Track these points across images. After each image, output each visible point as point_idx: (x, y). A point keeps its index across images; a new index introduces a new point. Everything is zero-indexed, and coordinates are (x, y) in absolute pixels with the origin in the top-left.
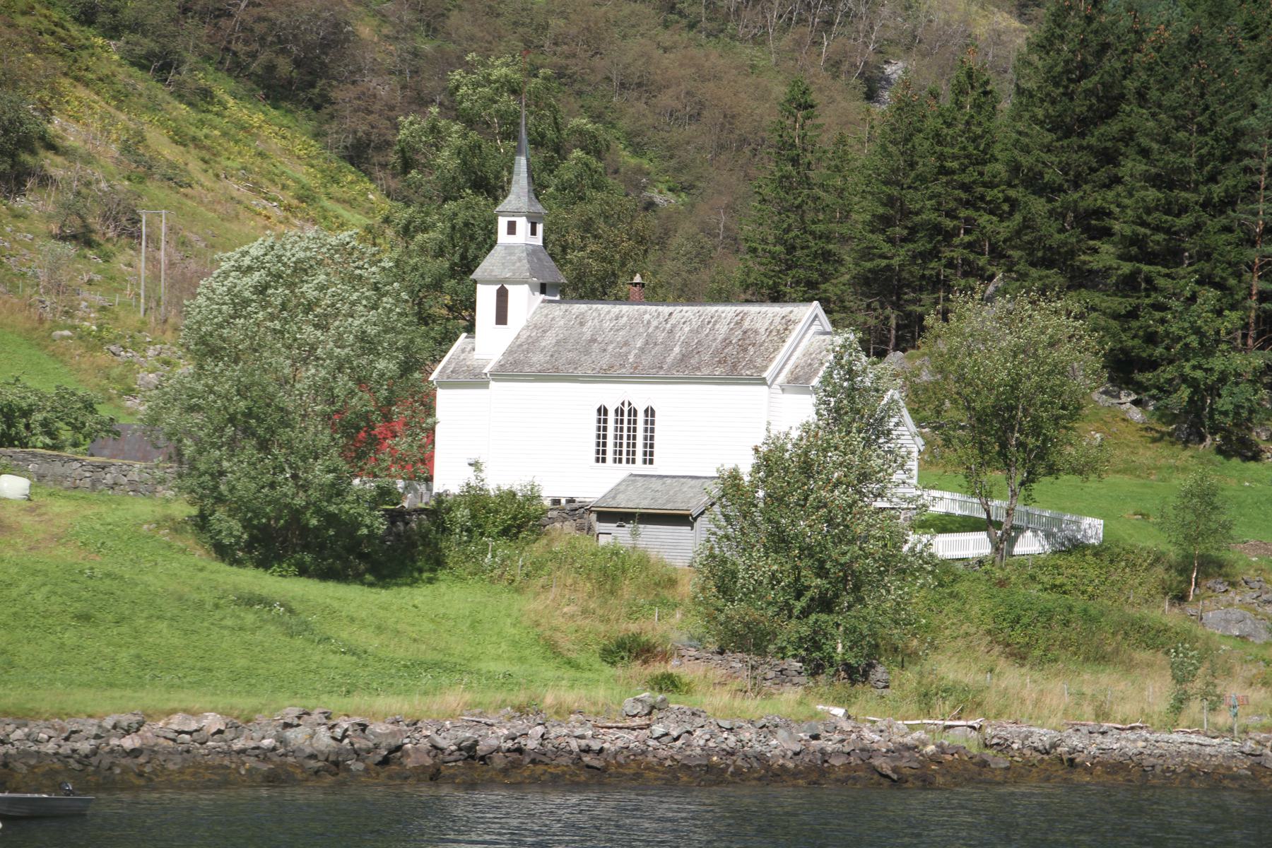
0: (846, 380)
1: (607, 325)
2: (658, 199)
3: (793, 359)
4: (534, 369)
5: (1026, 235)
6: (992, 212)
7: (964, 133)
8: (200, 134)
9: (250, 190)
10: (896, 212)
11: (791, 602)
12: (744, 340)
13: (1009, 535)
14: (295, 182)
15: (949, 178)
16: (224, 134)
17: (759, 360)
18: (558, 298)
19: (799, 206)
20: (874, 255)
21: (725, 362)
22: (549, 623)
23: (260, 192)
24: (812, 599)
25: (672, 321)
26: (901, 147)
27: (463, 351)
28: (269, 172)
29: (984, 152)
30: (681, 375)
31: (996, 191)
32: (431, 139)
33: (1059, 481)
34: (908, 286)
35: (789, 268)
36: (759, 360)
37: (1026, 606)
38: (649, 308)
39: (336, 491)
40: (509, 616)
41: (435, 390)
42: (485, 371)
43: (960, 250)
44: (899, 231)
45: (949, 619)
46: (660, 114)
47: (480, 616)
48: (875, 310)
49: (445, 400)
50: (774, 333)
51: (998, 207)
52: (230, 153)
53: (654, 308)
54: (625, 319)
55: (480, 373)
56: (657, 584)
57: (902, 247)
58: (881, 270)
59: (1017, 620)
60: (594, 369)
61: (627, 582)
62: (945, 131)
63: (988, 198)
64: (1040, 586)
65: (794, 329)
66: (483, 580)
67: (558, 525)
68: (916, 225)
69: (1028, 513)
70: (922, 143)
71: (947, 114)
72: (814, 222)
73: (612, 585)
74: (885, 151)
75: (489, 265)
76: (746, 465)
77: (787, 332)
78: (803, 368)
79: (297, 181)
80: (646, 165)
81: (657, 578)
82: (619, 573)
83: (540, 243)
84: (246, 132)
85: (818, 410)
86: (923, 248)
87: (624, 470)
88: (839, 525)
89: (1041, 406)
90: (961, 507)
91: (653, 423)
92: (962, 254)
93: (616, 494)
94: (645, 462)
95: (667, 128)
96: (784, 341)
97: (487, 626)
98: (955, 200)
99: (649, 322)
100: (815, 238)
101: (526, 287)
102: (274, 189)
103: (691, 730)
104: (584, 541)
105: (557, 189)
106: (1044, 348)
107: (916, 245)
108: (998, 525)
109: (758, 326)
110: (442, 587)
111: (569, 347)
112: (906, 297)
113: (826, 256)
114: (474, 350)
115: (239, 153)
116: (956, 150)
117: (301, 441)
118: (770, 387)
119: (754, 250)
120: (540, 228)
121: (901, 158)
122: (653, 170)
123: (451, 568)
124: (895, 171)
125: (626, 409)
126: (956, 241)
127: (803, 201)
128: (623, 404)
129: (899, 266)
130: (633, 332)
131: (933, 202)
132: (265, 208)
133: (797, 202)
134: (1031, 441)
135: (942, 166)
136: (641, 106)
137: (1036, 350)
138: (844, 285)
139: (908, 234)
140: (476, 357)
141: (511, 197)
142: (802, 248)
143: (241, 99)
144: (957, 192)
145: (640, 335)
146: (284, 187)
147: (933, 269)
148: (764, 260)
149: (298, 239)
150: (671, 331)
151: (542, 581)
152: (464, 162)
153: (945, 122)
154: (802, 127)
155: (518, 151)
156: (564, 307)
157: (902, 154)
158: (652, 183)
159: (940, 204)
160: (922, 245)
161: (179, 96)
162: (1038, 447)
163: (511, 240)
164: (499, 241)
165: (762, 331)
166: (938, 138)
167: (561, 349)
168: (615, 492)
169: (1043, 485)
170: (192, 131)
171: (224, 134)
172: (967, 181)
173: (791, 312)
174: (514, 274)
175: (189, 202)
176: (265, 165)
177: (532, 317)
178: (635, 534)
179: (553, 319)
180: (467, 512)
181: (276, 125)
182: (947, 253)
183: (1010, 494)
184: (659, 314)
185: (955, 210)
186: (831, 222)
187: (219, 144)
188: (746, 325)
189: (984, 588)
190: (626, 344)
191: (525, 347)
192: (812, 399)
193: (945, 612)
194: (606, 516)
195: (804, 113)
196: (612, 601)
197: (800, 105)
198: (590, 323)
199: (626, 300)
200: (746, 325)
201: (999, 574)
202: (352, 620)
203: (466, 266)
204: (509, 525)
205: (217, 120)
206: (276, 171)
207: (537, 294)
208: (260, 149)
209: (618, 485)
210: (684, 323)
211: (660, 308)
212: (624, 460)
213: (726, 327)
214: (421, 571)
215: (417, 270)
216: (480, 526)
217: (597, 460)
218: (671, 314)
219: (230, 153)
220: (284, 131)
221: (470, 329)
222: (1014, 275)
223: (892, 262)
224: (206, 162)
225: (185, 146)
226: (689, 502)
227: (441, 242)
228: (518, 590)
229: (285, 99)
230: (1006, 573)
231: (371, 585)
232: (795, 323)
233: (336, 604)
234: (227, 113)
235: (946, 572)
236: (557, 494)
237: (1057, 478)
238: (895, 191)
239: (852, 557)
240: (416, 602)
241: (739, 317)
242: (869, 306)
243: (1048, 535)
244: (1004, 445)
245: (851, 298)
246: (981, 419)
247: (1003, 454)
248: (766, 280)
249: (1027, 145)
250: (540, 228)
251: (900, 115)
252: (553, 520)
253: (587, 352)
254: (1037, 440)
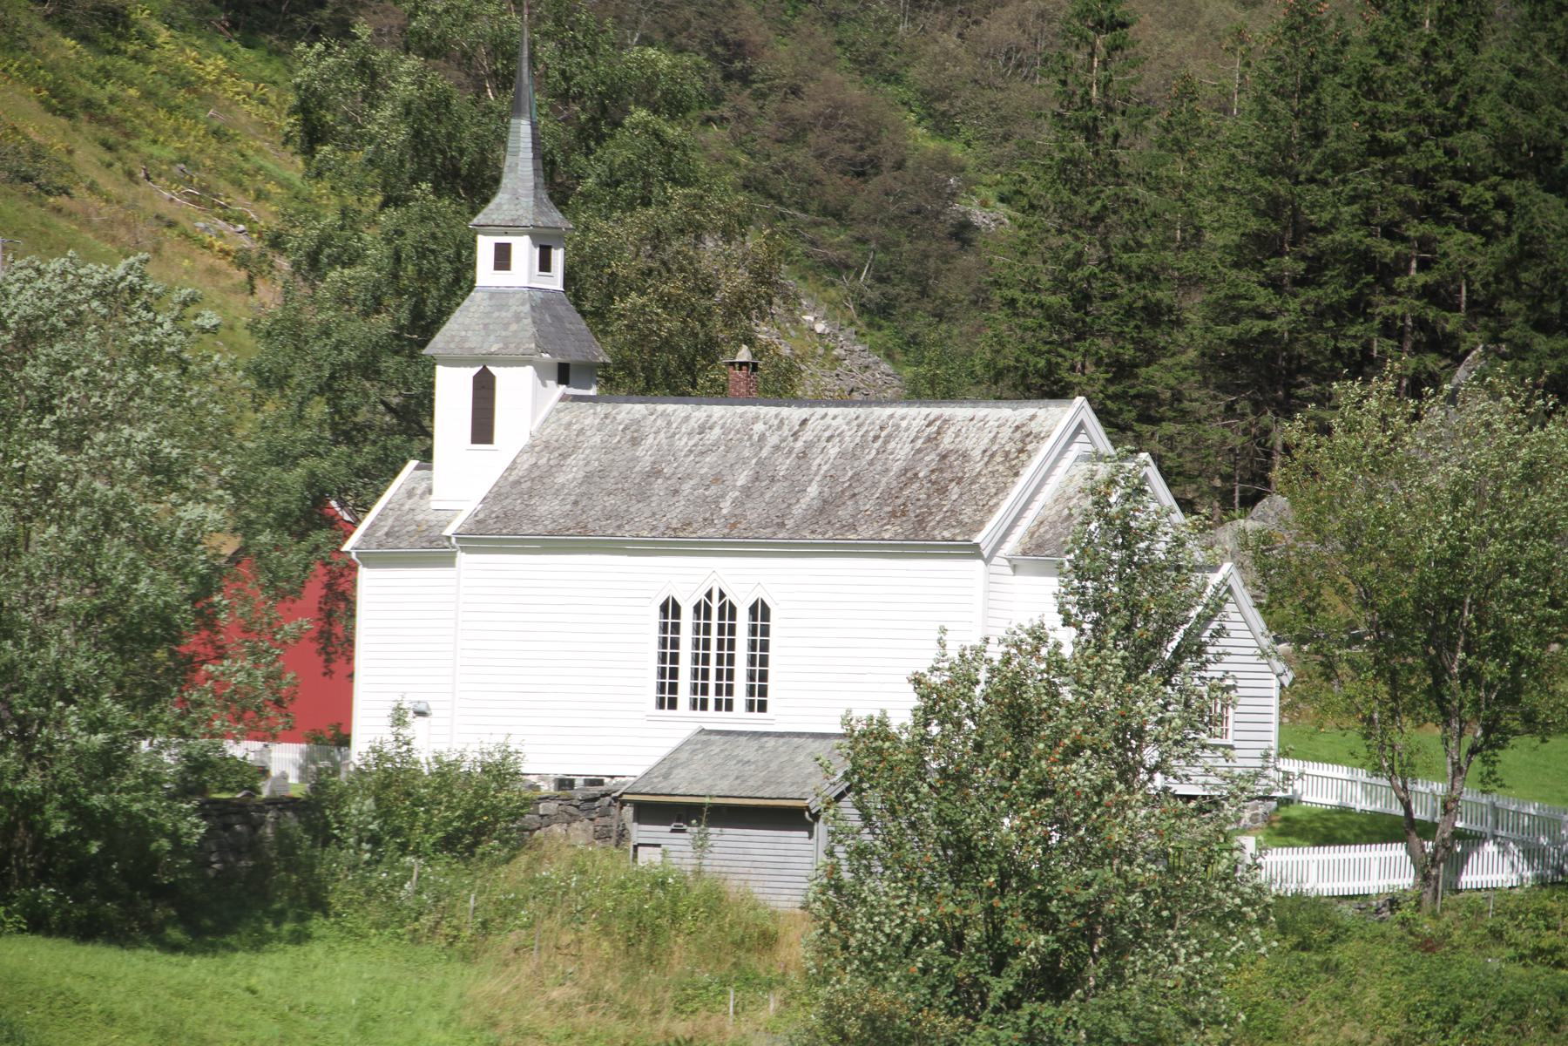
0: (1116, 547)
1: (682, 443)
2: (978, 216)
3: (1035, 508)
4: (540, 528)
5: (1526, 270)
6: (1474, 228)
7: (1418, 74)
8: (101, 95)
9: (195, 201)
10: (1285, 229)
11: (983, 978)
12: (941, 471)
13: (1449, 849)
14: (281, 186)
15: (1389, 161)
16: (148, 95)
17: (968, 511)
18: (593, 391)
19: (1098, 219)
20: (1240, 311)
21: (904, 513)
22: (515, 1020)
23: (214, 205)
24: (1026, 973)
25: (807, 436)
26: (1295, 102)
27: (410, 494)
28: (232, 168)
29: (1458, 110)
30: (818, 539)
31: (1479, 188)
32: (360, 86)
33: (1545, 747)
34: (1307, 370)
35: (1080, 337)
36: (968, 511)
37: (1474, 989)
38: (763, 410)
39: (110, 763)
40: (438, 1007)
41: (352, 568)
42: (448, 532)
43: (1410, 301)
44: (1289, 265)
45: (1317, 1013)
46: (987, 55)
47: (379, 1008)
48: (1243, 416)
49: (371, 585)
50: (999, 459)
51: (1486, 218)
52: (159, 132)
53: (773, 410)
54: (717, 431)
55: (440, 538)
56: (739, 944)
57: (1295, 296)
58: (1254, 340)
59: (1454, 1017)
60: (654, 528)
61: (680, 940)
62: (1382, 71)
63: (1465, 201)
64: (1511, 952)
65: (1036, 450)
66: (399, 937)
67: (557, 829)
68: (1323, 253)
69: (1495, 810)
70: (1335, 95)
71: (1387, 37)
72: (1126, 248)
73: (653, 945)
74: (1265, 110)
75: (461, 327)
76: (901, 710)
77: (1023, 457)
78: (1053, 525)
79: (285, 184)
80: (956, 150)
81: (739, 931)
82: (664, 922)
83: (559, 286)
84: (189, 91)
85: (1062, 605)
86: (1335, 298)
87: (713, 719)
88: (1077, 827)
89: (1509, 600)
90: (1368, 794)
91: (766, 631)
92: (1412, 309)
93: (671, 768)
94: (750, 707)
95: (999, 82)
96: (1017, 474)
97: (391, 1027)
98: (1400, 203)
99: (762, 438)
100: (1129, 279)
101: (529, 370)
102: (240, 198)
104: (602, 858)
105: (602, 184)
106: (1516, 486)
107: (1321, 292)
108: (1427, 830)
109: (969, 444)
110: (317, 951)
111: (609, 484)
112: (1300, 392)
113: (1154, 314)
114: (430, 491)
115: (176, 131)
116: (1401, 108)
117: (31, 667)
118: (987, 561)
119: (1012, 302)
120: (558, 257)
121: (1296, 124)
122: (972, 162)
123: (338, 915)
124: (1284, 149)
125: (715, 606)
126: (1401, 283)
127: (1104, 207)
128: (709, 595)
129: (1290, 332)
130: (732, 456)
131: (1355, 208)
132: (221, 236)
133: (1093, 210)
134: (1490, 667)
135: (1374, 138)
136: (950, 41)
137: (1498, 490)
138: (1184, 369)
139: (1307, 270)
140: (434, 505)
141: (501, 198)
142: (1104, 299)
143: (182, 29)
144: (1402, 188)
145: (745, 461)
146: (260, 196)
147: (1355, 337)
148: (1029, 322)
149: (34, 274)
150: (804, 455)
151: (512, 939)
152: (417, 134)
153: (1381, 54)
154: (1105, 65)
155: (516, 110)
156: (602, 409)
157: (1297, 116)
158: (969, 186)
159: (1370, 212)
160: (1333, 290)
161: (62, 22)
162: (1501, 679)
163: (502, 279)
164: (478, 284)
165: (977, 454)
166: (1368, 85)
167: (593, 490)
168: (669, 764)
169: (1517, 755)
170: (86, 89)
171: (148, 95)
172: (1421, 166)
173: (1033, 417)
174: (506, 346)
175: (63, 223)
176: (224, 155)
177: (541, 429)
178: (701, 846)
179: (581, 432)
180: (370, 803)
181: (248, 78)
182: (1383, 307)
183: (1450, 769)
184: (782, 422)
185: (1397, 224)
186: (1165, 248)
187: (138, 115)
188: (946, 442)
189: (1394, 952)
190: (717, 479)
191: (525, 486)
192: (1052, 584)
193: (1309, 1000)
194: (654, 811)
195: (1108, 37)
196: (649, 976)
197: (1100, 23)
198: (650, 440)
199: (720, 393)
200: (946, 442)
201: (1427, 927)
202: (110, 1018)
203: (425, 324)
204: (458, 830)
205: (136, 69)
206: (246, 166)
207: (552, 383)
208: (216, 123)
209: (677, 750)
210: (829, 439)
211: (785, 411)
212: (711, 704)
213: (908, 448)
214: (279, 918)
215: (328, 336)
216: (397, 832)
217: (661, 704)
218: (804, 422)
219: (159, 132)
220: (264, 89)
221: (427, 456)
222: (1504, 347)
223: (1274, 325)
224: (109, 148)
225: (71, 117)
226: (805, 784)
227: (377, 285)
228: (467, 958)
229: (269, 28)
230: (1442, 925)
231: (175, 948)
232: (1039, 438)
233: (82, 988)
234: (154, 55)
235: (1320, 922)
236: (562, 771)
237: (1544, 741)
238: (1282, 188)
239: (1101, 892)
240: (253, 981)
241: (934, 429)
242: (1230, 407)
243: (1531, 853)
244: (1437, 670)
245: (1195, 395)
246: (1390, 627)
247: (1436, 694)
248: (1032, 359)
249: (1530, 95)
250: (558, 257)
251: (1292, 39)
252: (547, 820)
253: (643, 496)
254: (1501, 667)
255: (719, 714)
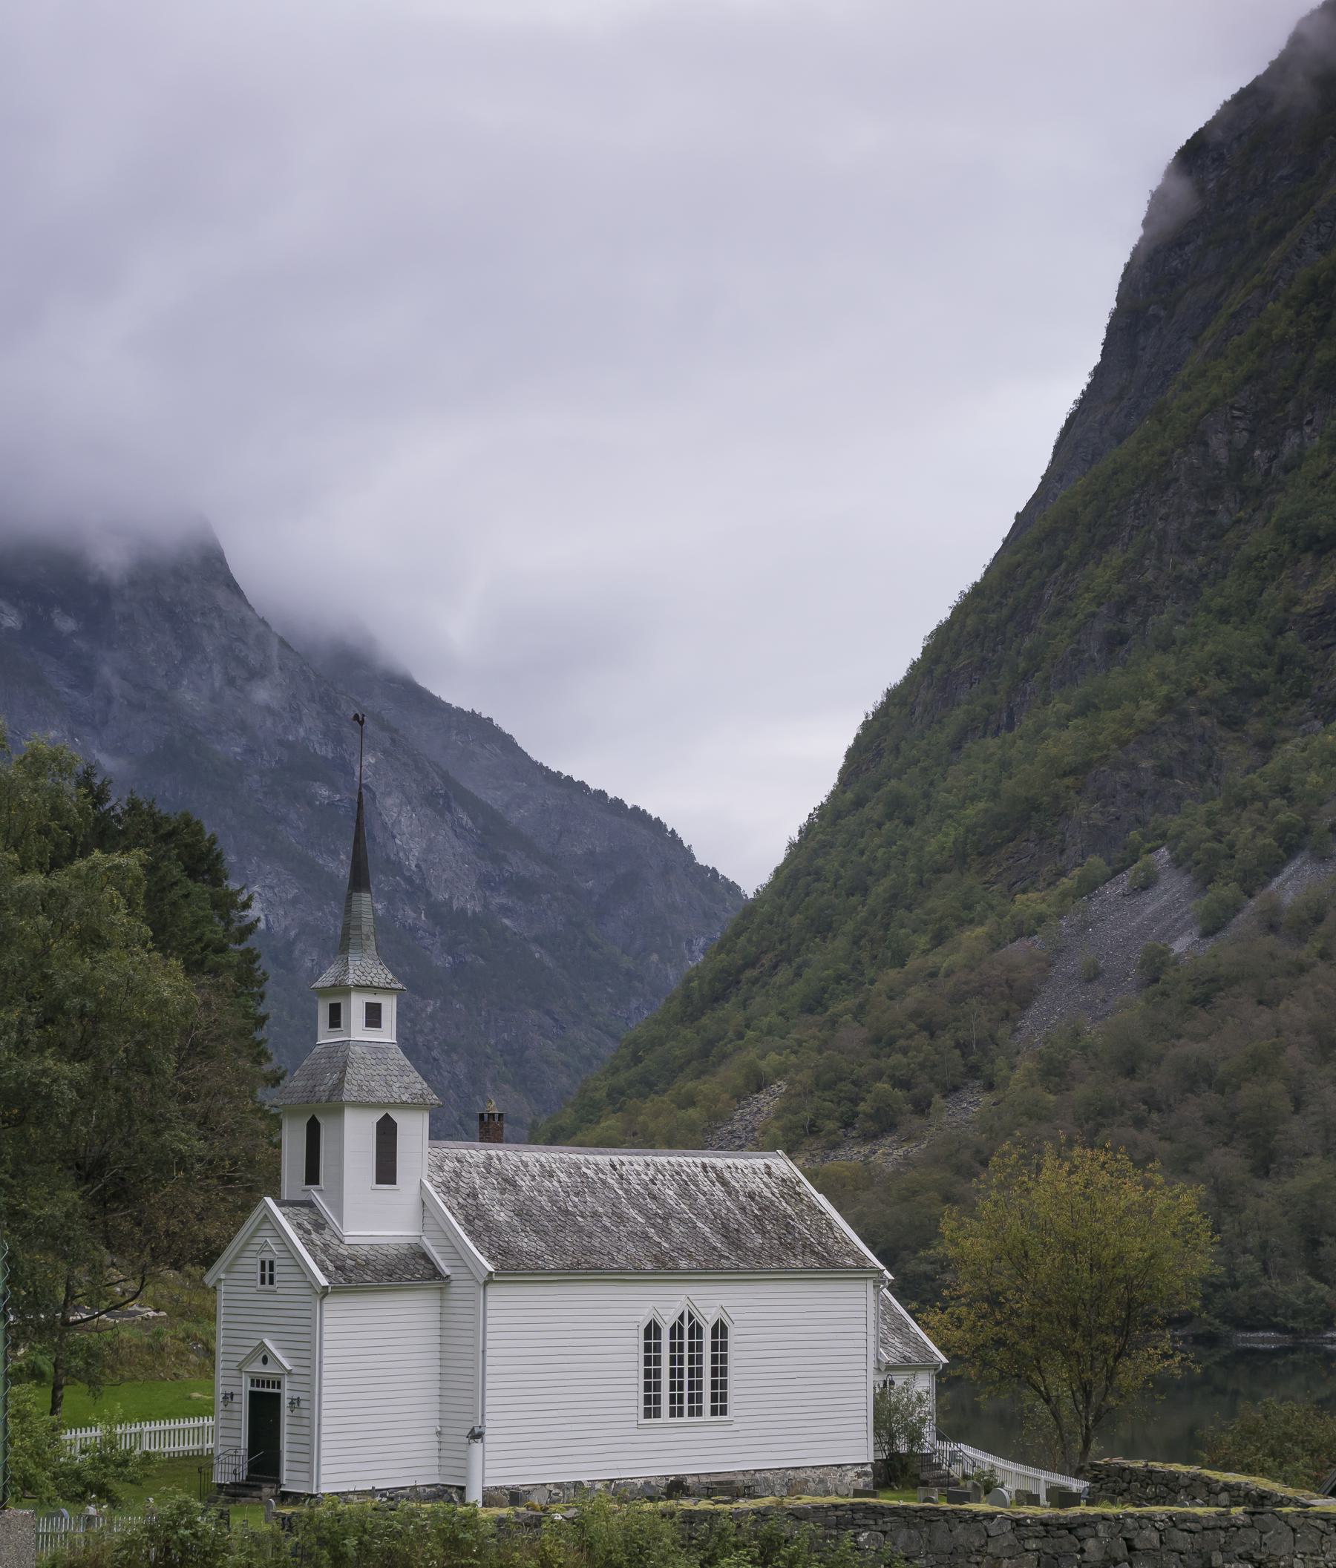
103: (1277, 1536)
125: (686, 1327)
163: (373, 1036)
217: (647, 1414)
255: (715, 1418)
